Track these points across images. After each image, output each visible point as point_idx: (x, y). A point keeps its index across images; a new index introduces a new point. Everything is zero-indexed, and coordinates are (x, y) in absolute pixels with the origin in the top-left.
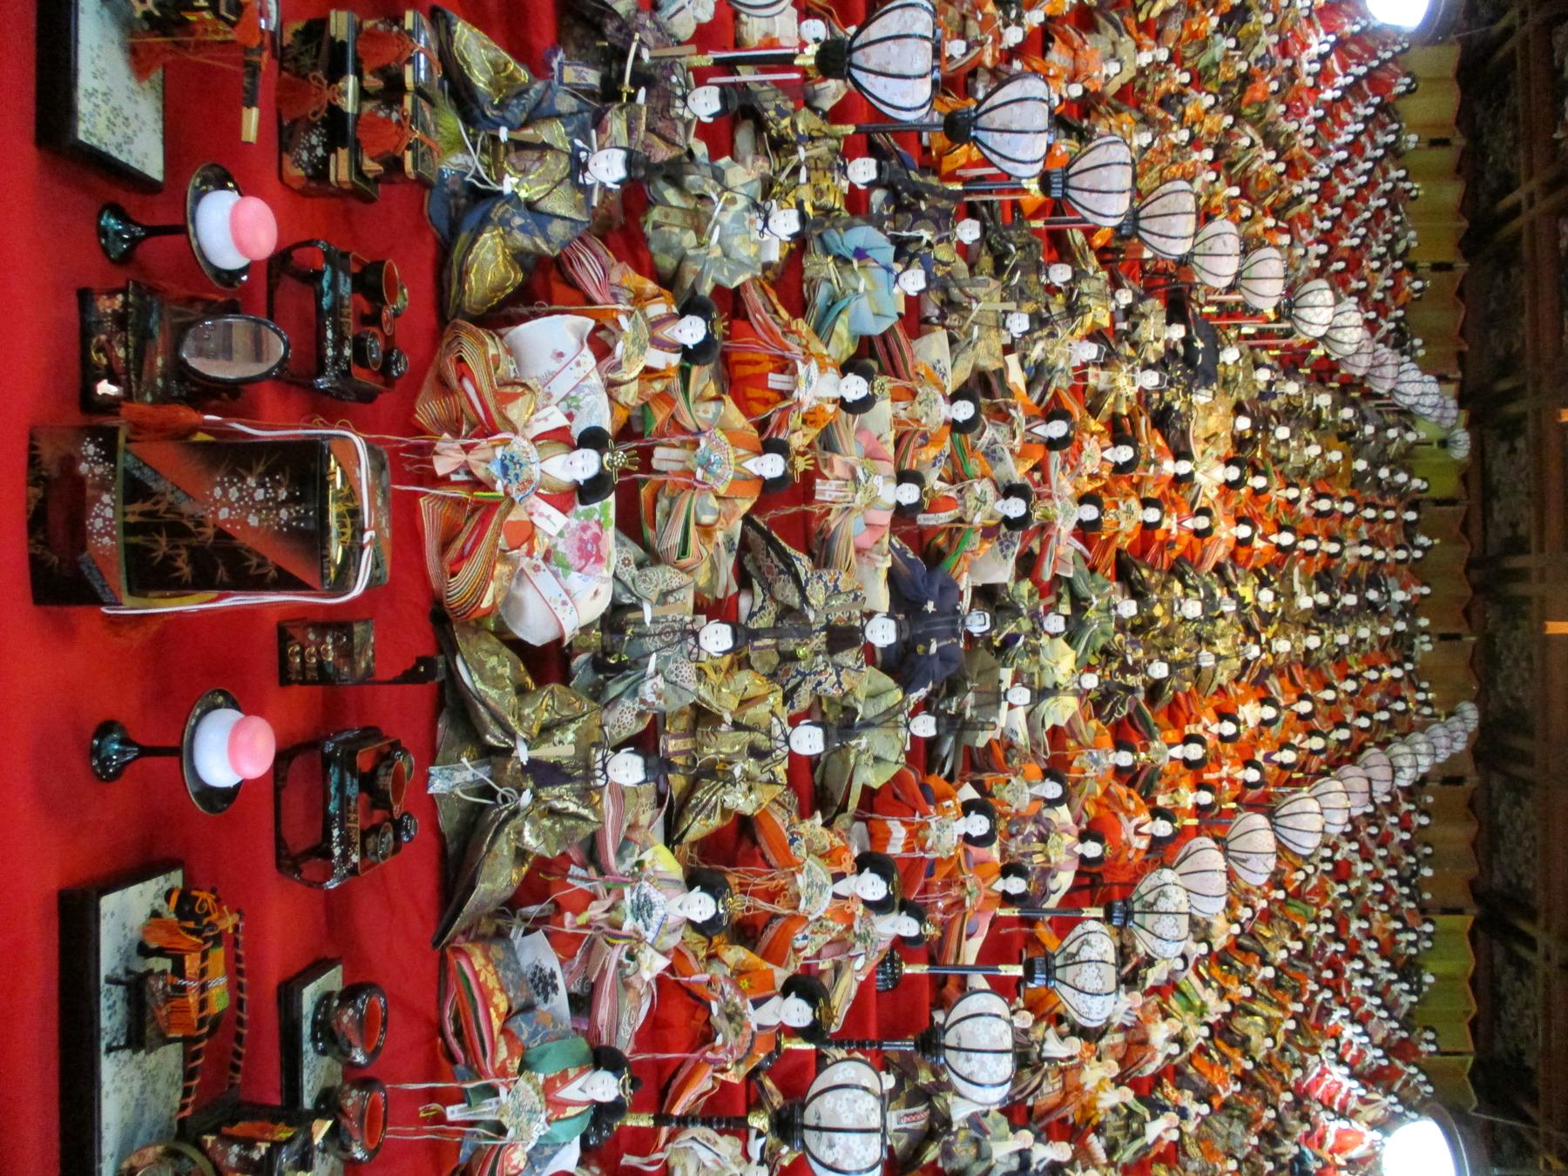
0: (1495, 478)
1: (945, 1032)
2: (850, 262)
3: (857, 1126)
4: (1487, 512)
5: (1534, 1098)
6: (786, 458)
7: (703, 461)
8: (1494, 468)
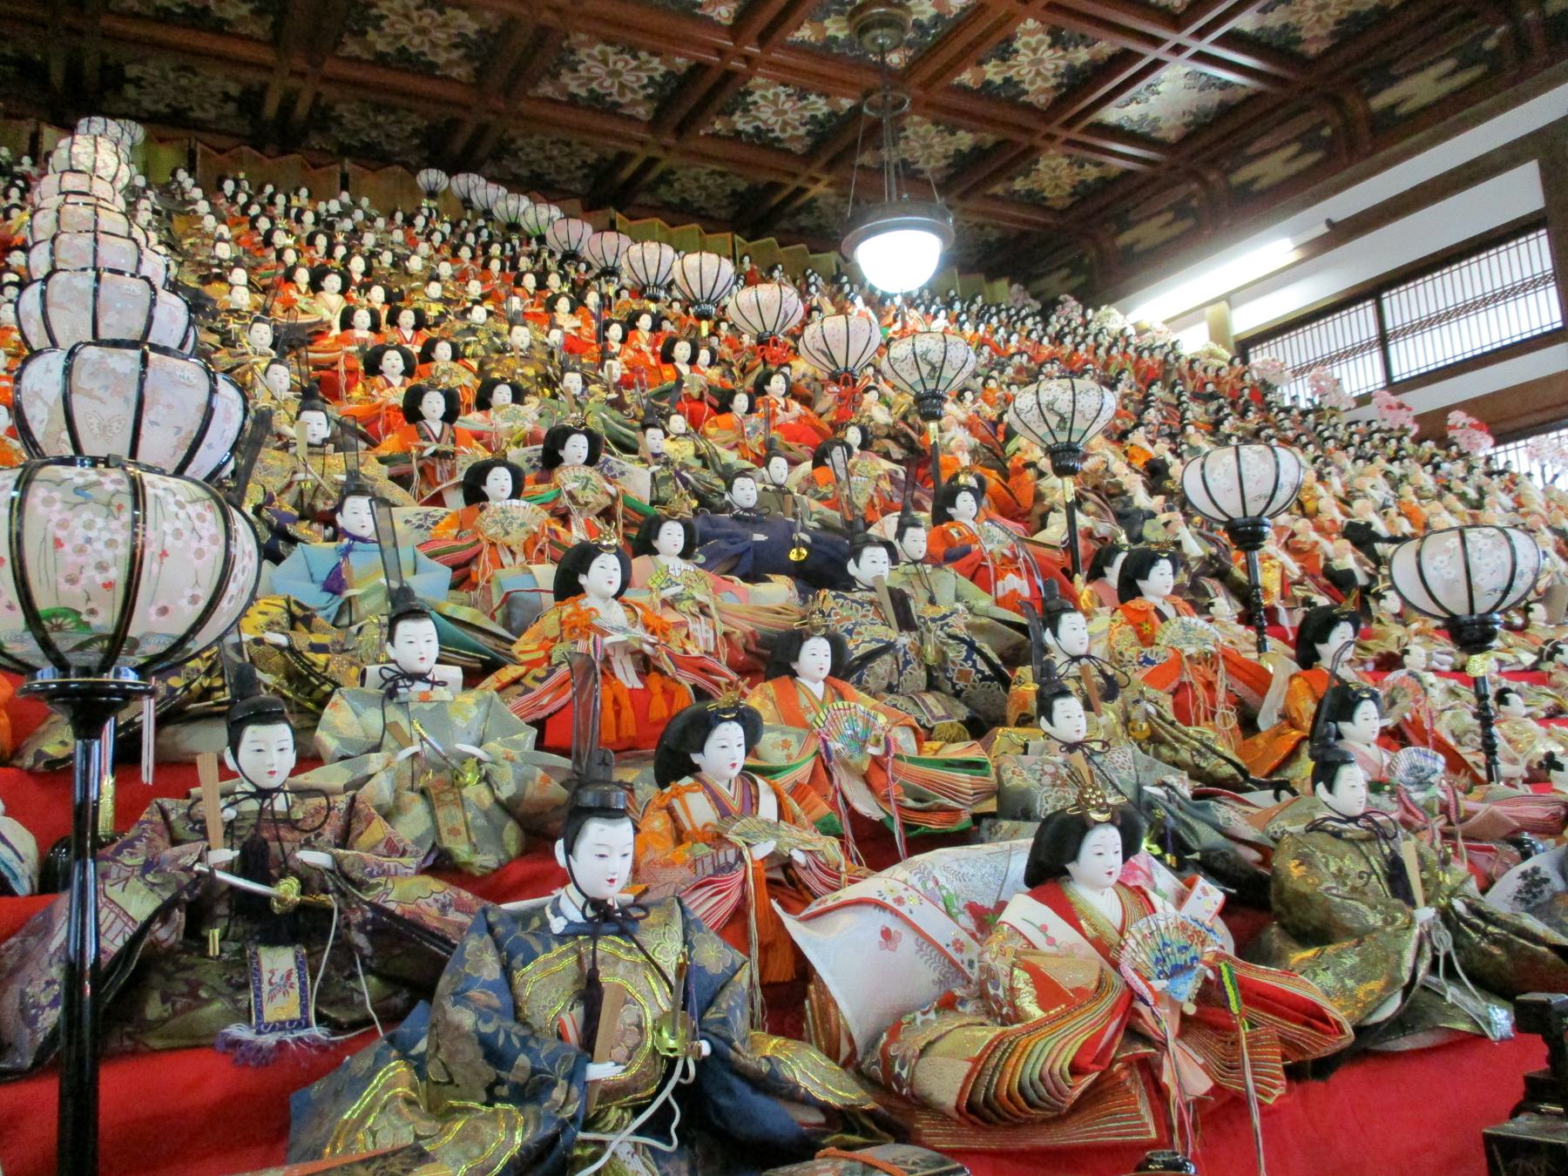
0: (161, 107)
1: (1231, 519)
2: (349, 601)
3: (1473, 560)
4: (200, 126)
5: (774, 187)
6: (809, 636)
7: (854, 745)
8: (152, 108)
